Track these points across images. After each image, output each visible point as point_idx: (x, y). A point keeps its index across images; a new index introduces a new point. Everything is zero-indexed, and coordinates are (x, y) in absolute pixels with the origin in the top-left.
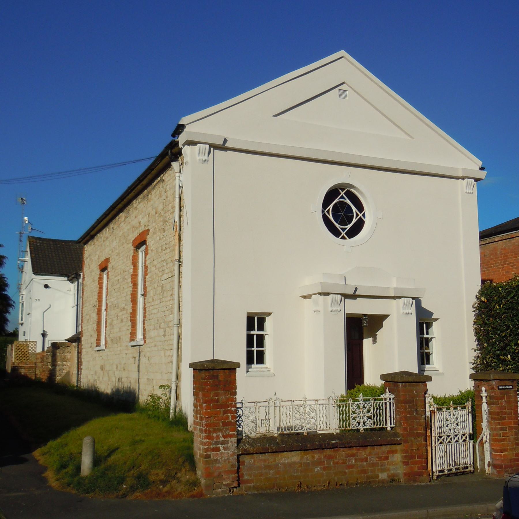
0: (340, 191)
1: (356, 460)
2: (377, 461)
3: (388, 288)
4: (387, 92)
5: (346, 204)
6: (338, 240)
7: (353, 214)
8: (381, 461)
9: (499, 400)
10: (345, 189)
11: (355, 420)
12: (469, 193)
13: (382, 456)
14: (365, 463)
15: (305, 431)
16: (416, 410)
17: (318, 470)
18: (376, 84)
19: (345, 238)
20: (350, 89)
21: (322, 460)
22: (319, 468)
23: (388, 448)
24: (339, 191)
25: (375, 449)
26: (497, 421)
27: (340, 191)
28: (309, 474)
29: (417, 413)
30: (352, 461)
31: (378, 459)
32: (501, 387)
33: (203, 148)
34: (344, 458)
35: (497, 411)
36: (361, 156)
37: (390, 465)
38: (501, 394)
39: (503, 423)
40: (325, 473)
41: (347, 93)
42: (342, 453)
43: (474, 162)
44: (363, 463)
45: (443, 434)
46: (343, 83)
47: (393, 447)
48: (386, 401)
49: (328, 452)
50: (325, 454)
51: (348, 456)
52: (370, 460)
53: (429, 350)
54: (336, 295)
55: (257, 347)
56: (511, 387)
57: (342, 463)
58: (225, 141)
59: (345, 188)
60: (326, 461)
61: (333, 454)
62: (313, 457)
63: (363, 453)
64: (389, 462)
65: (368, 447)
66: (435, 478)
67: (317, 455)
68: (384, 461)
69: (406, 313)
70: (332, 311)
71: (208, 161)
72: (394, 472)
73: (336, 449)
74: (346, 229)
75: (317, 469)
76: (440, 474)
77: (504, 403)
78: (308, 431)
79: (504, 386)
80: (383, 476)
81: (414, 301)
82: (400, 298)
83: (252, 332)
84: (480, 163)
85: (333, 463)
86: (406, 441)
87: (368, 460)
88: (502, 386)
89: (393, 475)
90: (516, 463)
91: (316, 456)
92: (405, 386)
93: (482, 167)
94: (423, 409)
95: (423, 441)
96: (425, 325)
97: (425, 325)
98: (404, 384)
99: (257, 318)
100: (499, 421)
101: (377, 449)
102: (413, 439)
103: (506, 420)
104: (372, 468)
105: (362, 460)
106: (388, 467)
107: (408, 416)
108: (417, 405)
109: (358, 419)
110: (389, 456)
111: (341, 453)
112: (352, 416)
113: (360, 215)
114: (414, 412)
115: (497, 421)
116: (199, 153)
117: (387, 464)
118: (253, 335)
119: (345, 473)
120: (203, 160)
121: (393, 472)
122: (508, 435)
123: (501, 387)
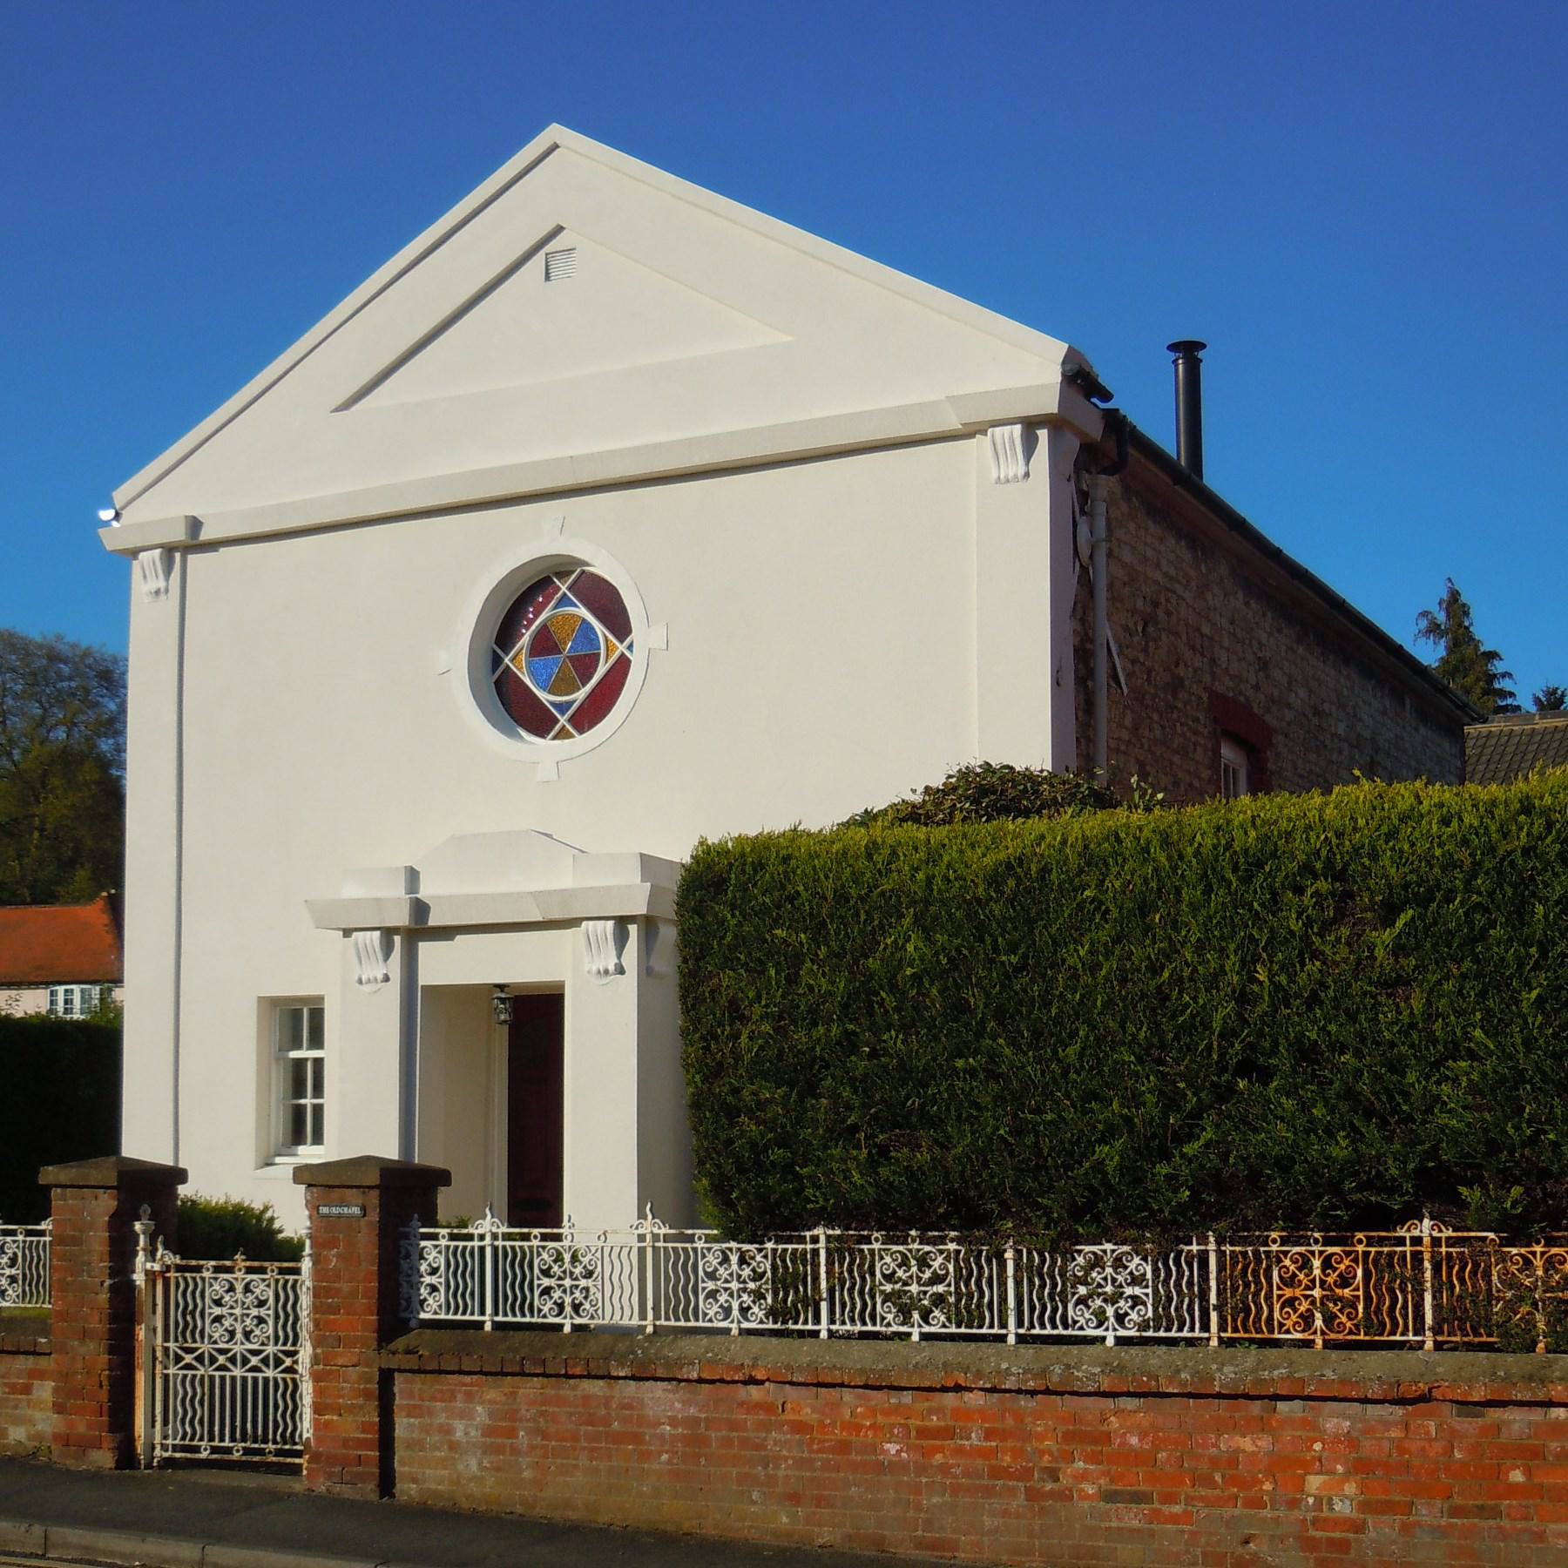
2: (5, 1393)
19: (569, 736)
31: (7, 1390)
36: (571, 457)
48: (482, 1244)
53: (322, 1097)
54: (369, 933)
58: (195, 525)
76: (178, 1455)
77: (335, 1260)
82: (573, 923)
109: (723, 1298)
112: (1074, 1294)
113: (622, 648)
116: (145, 577)
121: (40, 1428)
122: (341, 1361)
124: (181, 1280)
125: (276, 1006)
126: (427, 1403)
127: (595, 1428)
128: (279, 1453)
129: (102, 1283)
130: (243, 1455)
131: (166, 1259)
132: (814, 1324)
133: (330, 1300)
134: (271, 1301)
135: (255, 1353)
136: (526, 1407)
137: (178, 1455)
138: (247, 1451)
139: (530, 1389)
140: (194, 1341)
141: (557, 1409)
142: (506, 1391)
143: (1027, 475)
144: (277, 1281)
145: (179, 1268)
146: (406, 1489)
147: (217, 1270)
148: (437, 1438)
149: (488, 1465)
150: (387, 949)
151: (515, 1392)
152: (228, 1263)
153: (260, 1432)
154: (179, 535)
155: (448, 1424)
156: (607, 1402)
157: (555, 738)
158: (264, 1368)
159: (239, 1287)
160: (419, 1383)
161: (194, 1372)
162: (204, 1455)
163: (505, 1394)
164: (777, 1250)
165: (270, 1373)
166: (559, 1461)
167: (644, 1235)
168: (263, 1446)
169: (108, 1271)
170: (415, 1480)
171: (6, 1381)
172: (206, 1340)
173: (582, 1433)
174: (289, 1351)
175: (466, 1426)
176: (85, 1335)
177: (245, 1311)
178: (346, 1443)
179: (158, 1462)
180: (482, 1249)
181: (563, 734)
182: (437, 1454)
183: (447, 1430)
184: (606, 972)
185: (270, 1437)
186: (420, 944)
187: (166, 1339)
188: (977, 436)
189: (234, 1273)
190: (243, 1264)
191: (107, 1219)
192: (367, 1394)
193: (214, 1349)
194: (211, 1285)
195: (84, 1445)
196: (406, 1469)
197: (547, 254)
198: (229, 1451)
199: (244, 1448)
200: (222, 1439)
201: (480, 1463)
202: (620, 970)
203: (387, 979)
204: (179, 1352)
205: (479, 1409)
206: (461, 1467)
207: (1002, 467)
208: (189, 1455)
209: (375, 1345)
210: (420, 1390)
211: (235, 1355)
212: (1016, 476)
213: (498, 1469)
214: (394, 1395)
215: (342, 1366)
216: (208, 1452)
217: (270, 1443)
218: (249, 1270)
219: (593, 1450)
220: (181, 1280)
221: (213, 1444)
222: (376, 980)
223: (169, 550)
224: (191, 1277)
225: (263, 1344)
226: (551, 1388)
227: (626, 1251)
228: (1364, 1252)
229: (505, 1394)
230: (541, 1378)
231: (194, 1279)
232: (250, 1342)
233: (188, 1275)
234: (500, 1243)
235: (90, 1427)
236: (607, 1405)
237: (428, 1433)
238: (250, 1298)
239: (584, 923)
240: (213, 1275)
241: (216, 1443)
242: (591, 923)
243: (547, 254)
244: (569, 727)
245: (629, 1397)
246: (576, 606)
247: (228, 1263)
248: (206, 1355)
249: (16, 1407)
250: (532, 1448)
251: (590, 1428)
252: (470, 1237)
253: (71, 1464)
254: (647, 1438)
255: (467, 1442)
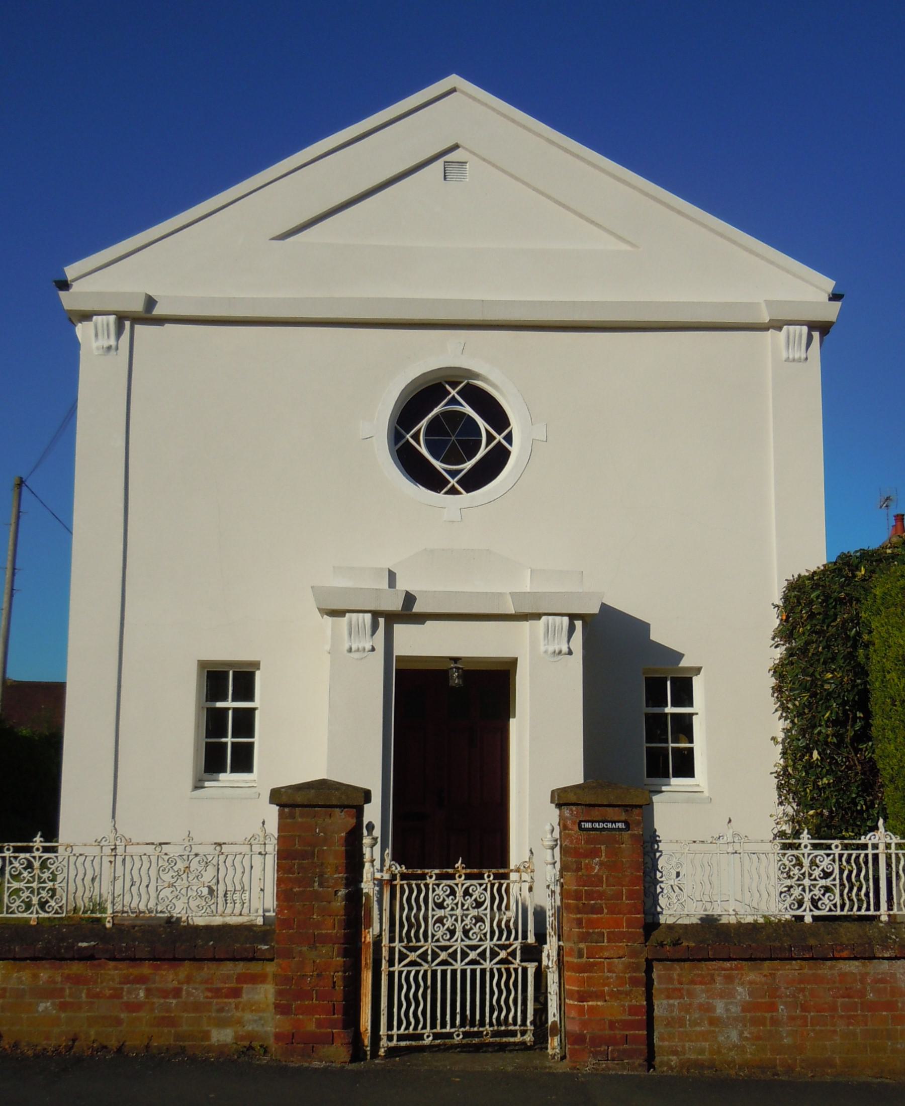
0: (448, 387)
1: (148, 991)
2: (207, 997)
3: (501, 593)
4: (566, 150)
5: (463, 414)
6: (440, 498)
7: (480, 435)
8: (219, 1000)
9: (582, 860)
10: (462, 382)
11: (475, 900)
12: (794, 360)
13: (223, 988)
14: (174, 1001)
15: (34, 916)
16: (321, 876)
17: (46, 1008)
18: (539, 135)
20: (475, 158)
21: (59, 986)
22: (49, 1004)
23: (241, 968)
24: (445, 387)
25: (204, 968)
26: (574, 916)
27: (448, 387)
28: (23, 1015)
29: (320, 885)
30: (138, 994)
31: (210, 994)
32: (588, 825)
33: (103, 325)
34: (118, 986)
35: (576, 888)
36: (483, 301)
37: (243, 1010)
38: (587, 842)
39: (591, 923)
40: (63, 1015)
41: (467, 167)
42: (112, 972)
43: (812, 284)
44: (167, 1001)
45: (422, 943)
46: (456, 147)
47: (255, 968)
49: (76, 968)
50: (67, 972)
51: (126, 980)
52: (189, 994)
54: (361, 615)
55: (233, 737)
56: (621, 825)
57: (112, 997)
58: (151, 302)
59: (459, 380)
60: (70, 988)
61: (90, 973)
62: (35, 977)
63: (171, 977)
64: (240, 1003)
65: (186, 962)
66: (382, 1052)
67: (45, 974)
68: (226, 1000)
69: (555, 652)
70: (350, 650)
71: (117, 348)
72: (256, 1029)
73: (96, 962)
74: (459, 471)
75: (44, 1006)
76: (403, 1044)
78: (40, 916)
79: (599, 822)
80: (222, 1036)
81: (579, 624)
82: (537, 616)
83: (219, 705)
84: (829, 284)
85: (88, 996)
86: (287, 954)
87: (184, 993)
88: (592, 822)
89: (251, 1037)
90: (632, 1032)
91: (44, 975)
92: (292, 816)
93: (834, 293)
94: (341, 875)
95: (338, 956)
96: (669, 683)
97: (669, 683)
98: (287, 810)
99: (234, 672)
100: (579, 916)
101: (208, 970)
102: (305, 949)
103: (602, 913)
104: (194, 1015)
105: (165, 994)
106: (239, 1014)
107: (295, 890)
108: (322, 864)
110: (242, 987)
111: (109, 972)
113: (499, 438)
114: (314, 881)
115: (574, 916)
117: (237, 1008)
118: (228, 709)
119: (118, 1022)
120: (103, 348)
121: (250, 1028)
122: (606, 954)
123: (588, 825)
124: (405, 886)
125: (205, 668)
126: (686, 987)
127: (851, 1000)
128: (495, 1034)
129: (336, 892)
130: (463, 1038)
131: (394, 868)
132: (875, 910)
133: (592, 902)
134: (488, 902)
135: (473, 948)
136: (786, 985)
137: (403, 1044)
138: (466, 1035)
139: (789, 971)
140: (418, 940)
141: (814, 986)
142: (766, 972)
143: (807, 359)
144: (493, 885)
145: (404, 877)
146: (668, 1061)
147: (440, 877)
148: (697, 1016)
149: (748, 1035)
150: (375, 627)
151: (774, 974)
152: (450, 871)
153: (478, 1017)
154: (138, 307)
155: (708, 1003)
156: (864, 976)
157: (446, 493)
158: (482, 961)
159: (460, 892)
160: (676, 971)
161: (418, 968)
162: (427, 1041)
163: (765, 976)
164: (843, 854)
165: (487, 965)
166: (818, 1028)
167: (890, 844)
168: (481, 1029)
169: (344, 882)
170: (675, 1053)
171: (209, 986)
172: (430, 939)
173: (839, 1004)
174: (503, 945)
175: (726, 1004)
176: (315, 941)
177: (466, 912)
178: (612, 1025)
179: (385, 1051)
180: (876, 857)
181: (453, 491)
182: (698, 1029)
183: (708, 1008)
184: (560, 652)
185: (487, 1020)
186: (395, 625)
187: (392, 940)
188: (771, 330)
189: (455, 879)
190: (464, 871)
191: (343, 834)
192: (634, 982)
193: (437, 947)
194: (434, 890)
195: (312, 1043)
196: (666, 1043)
197: (445, 162)
198: (450, 1036)
199: (464, 1033)
200: (443, 1026)
201: (741, 1034)
202: (570, 653)
203: (373, 649)
204: (405, 951)
205: (740, 989)
206: (721, 1039)
207: (790, 350)
208: (413, 1043)
209: (642, 939)
210: (679, 975)
211: (456, 951)
212: (800, 358)
213: (758, 1038)
214: (653, 980)
215: (606, 958)
216: (431, 1038)
217: (487, 1027)
218: (468, 877)
219: (849, 1017)
220: (405, 886)
221: (434, 1031)
222: (364, 649)
223: (121, 318)
224: (407, 884)
225: (481, 940)
226: (807, 969)
227: (89, 859)
228: (839, 854)
229: (765, 976)
230: (799, 961)
231: (418, 886)
232: (470, 939)
233: (414, 883)
234: (870, 851)
235: (319, 1024)
236: (862, 981)
237: (688, 1011)
238: (469, 901)
239: (544, 618)
240: (437, 882)
241: (438, 1029)
242: (551, 618)
243: (445, 162)
244: (457, 486)
245: (883, 973)
246: (461, 405)
247: (450, 871)
248: (430, 952)
249: (221, 1010)
250: (792, 1018)
251: (847, 1000)
252: (865, 847)
253: (295, 1062)
254: (900, 1005)
255: (728, 1018)
